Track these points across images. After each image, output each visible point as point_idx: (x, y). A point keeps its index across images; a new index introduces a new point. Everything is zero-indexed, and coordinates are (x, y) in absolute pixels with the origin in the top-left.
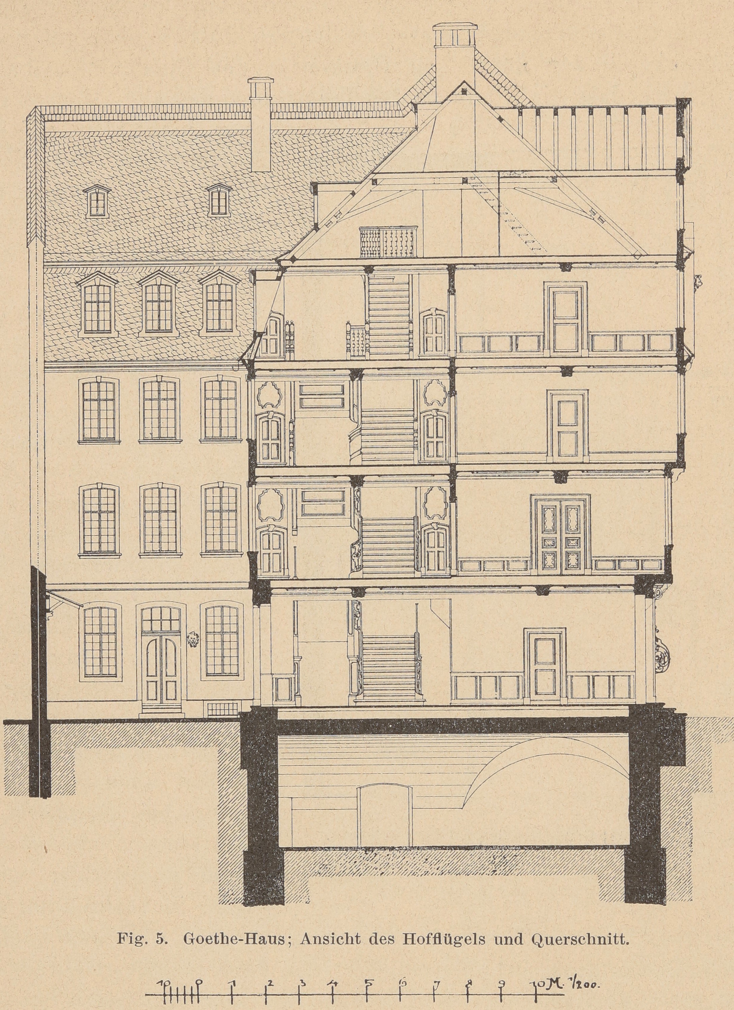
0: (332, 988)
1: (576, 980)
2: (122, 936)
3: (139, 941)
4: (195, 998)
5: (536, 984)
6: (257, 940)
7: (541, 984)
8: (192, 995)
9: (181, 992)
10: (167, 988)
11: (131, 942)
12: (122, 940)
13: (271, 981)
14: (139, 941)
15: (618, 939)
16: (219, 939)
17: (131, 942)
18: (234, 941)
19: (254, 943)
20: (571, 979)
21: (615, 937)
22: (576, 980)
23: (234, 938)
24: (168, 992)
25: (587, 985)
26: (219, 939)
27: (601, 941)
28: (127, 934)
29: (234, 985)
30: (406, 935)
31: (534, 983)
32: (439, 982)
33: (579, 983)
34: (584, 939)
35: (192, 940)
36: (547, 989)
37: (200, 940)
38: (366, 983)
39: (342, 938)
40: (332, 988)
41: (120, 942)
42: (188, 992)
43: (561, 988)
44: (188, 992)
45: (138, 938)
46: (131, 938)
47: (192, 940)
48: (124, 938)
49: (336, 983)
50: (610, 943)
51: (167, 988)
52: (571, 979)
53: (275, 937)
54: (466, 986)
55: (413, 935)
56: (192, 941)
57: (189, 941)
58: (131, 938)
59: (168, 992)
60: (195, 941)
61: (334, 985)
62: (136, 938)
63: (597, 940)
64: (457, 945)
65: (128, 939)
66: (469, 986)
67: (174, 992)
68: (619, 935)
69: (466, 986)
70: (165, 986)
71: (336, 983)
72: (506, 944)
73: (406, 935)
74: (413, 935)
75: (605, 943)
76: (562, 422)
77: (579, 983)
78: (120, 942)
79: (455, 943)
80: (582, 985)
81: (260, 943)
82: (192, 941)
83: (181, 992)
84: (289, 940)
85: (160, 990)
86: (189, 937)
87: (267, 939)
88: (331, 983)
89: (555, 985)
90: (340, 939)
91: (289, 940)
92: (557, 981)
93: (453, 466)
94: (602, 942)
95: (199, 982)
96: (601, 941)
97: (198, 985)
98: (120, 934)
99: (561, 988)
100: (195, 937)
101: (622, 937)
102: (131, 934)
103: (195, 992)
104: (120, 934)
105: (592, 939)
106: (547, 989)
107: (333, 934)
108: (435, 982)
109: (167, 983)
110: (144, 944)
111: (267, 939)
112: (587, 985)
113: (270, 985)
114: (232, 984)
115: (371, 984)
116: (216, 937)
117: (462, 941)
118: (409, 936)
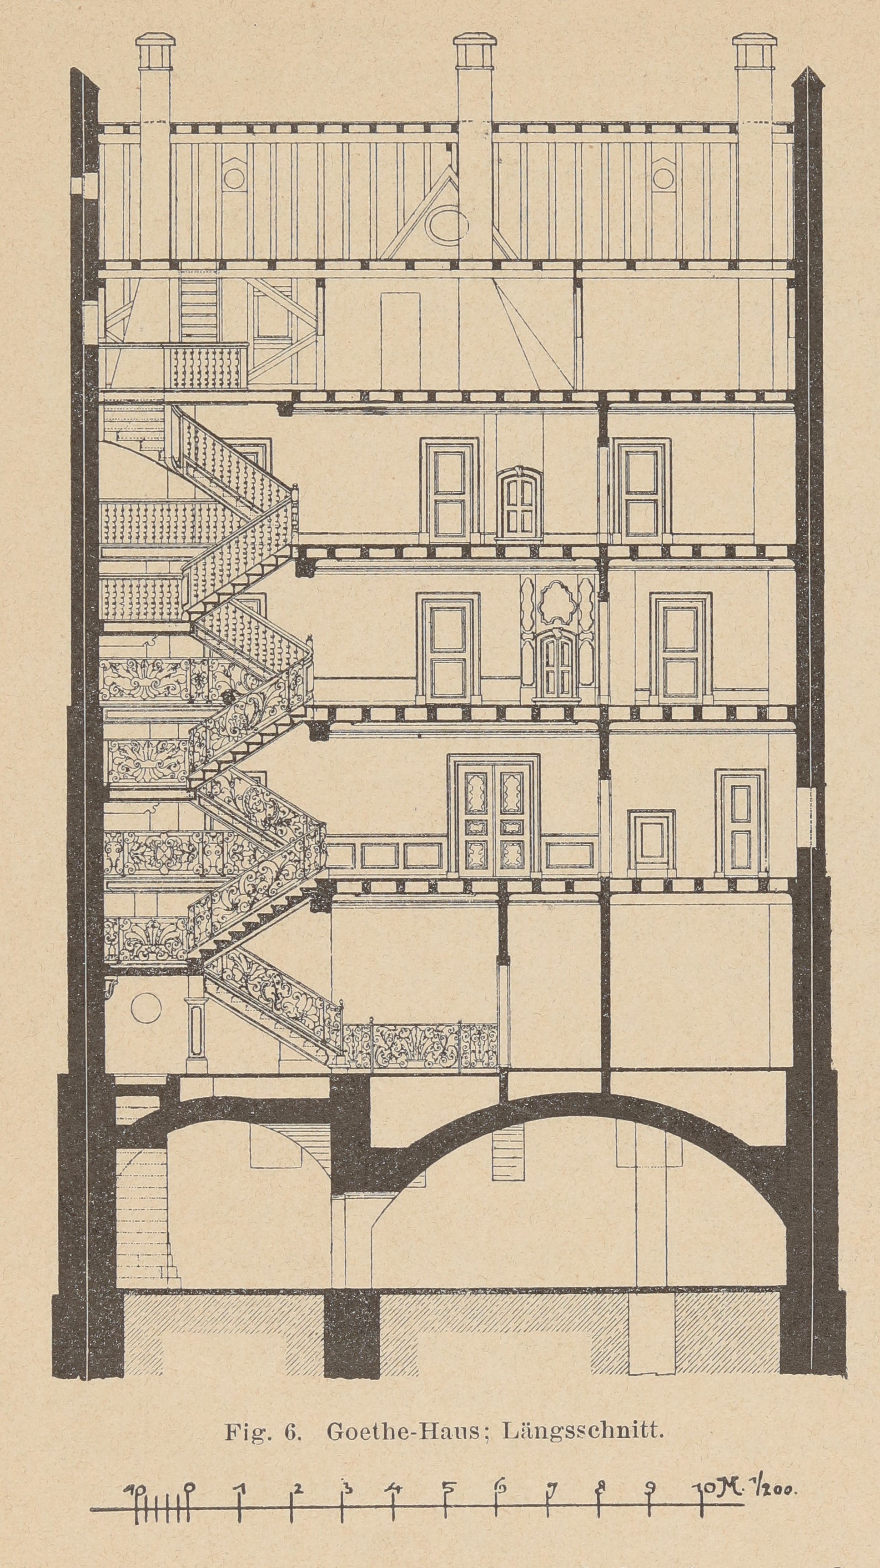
0: (239, 1494)
1: (762, 1483)
2: (232, 1430)
3: (257, 1436)
4: (183, 1513)
5: (702, 1488)
6: (439, 1433)
7: (710, 1488)
8: (179, 1509)
9: (162, 1504)
10: (141, 1499)
11: (246, 1439)
12: (232, 1434)
13: (299, 1486)
14: (257, 1436)
15: (648, 1430)
16: (380, 1432)
17: (246, 1439)
18: (404, 1435)
19: (434, 1437)
20: (754, 1479)
21: (643, 1426)
22: (762, 1483)
23: (403, 1430)
24: (141, 1504)
25: (778, 1490)
26: (380, 1432)
27: (623, 1432)
28: (239, 1425)
29: (244, 1492)
30: (424, 1425)
31: (699, 1486)
32: (555, 1485)
33: (766, 1486)
34: (597, 1429)
35: (340, 1434)
36: (719, 1496)
37: (352, 1434)
38: (444, 1487)
39: (597, 1429)
40: (239, 1494)
41: (229, 1438)
42: (173, 1504)
43: (740, 1494)
44: (173, 1504)
45: (258, 1432)
46: (246, 1430)
47: (340, 1434)
48: (234, 1432)
49: (398, 1489)
50: (636, 1436)
51: (141, 1499)
52: (754, 1479)
53: (465, 1429)
54: (597, 1491)
55: (434, 1424)
56: (340, 1436)
57: (335, 1435)
58: (246, 1430)
59: (141, 1504)
60: (344, 1435)
61: (395, 1491)
62: (254, 1432)
63: (616, 1432)
64: (554, 1439)
65: (241, 1433)
66: (601, 1491)
67: (151, 1505)
68: (648, 1424)
69: (597, 1491)
70: (137, 1495)
71: (398, 1489)
72: (620, 1436)
73: (424, 1425)
74: (434, 1424)
75: (627, 1436)
76: (367, 863)
77: (766, 1486)
78: (229, 1438)
79: (553, 1437)
80: (771, 1490)
81: (442, 1436)
82: (340, 1436)
83: (162, 1504)
84: (487, 1433)
85: (128, 1501)
86: (335, 1428)
87: (453, 1432)
88: (390, 1488)
89: (729, 1490)
90: (594, 1429)
91: (487, 1433)
92: (732, 1484)
93: (503, 883)
94: (624, 1434)
95: (189, 1488)
96: (623, 1432)
97: (188, 1492)
98: (229, 1426)
99: (740, 1494)
100: (344, 1430)
101: (653, 1426)
102: (246, 1425)
103: (183, 1504)
104: (229, 1426)
105: (608, 1431)
106: (719, 1496)
107: (635, 1422)
108: (549, 1485)
109: (140, 1491)
110: (266, 1440)
111: (453, 1432)
112: (778, 1490)
113: (298, 1492)
114: (240, 1490)
115: (452, 1490)
116: (375, 1428)
117: (563, 1433)
118: (429, 1427)
